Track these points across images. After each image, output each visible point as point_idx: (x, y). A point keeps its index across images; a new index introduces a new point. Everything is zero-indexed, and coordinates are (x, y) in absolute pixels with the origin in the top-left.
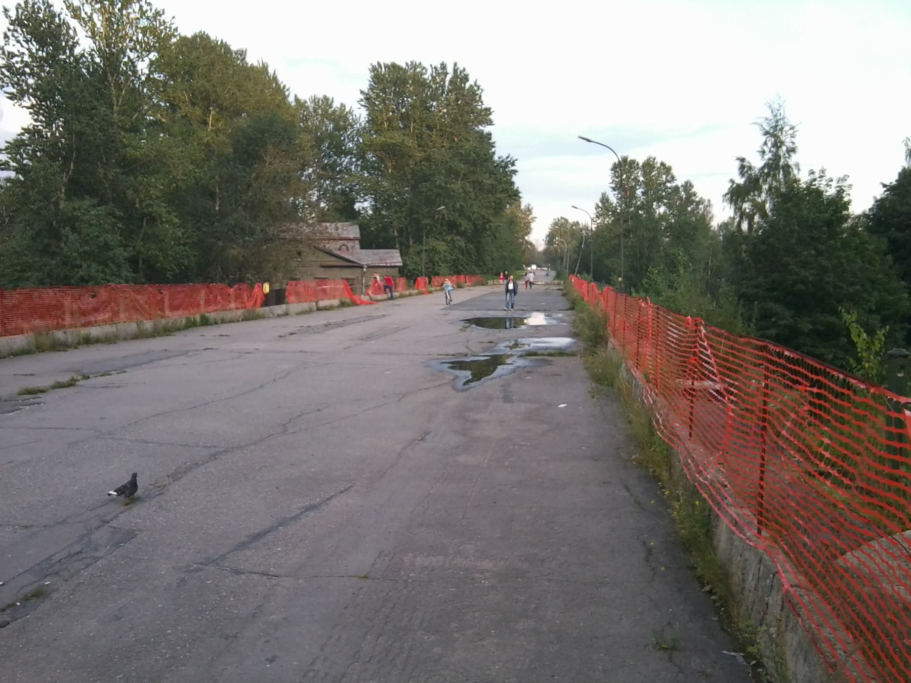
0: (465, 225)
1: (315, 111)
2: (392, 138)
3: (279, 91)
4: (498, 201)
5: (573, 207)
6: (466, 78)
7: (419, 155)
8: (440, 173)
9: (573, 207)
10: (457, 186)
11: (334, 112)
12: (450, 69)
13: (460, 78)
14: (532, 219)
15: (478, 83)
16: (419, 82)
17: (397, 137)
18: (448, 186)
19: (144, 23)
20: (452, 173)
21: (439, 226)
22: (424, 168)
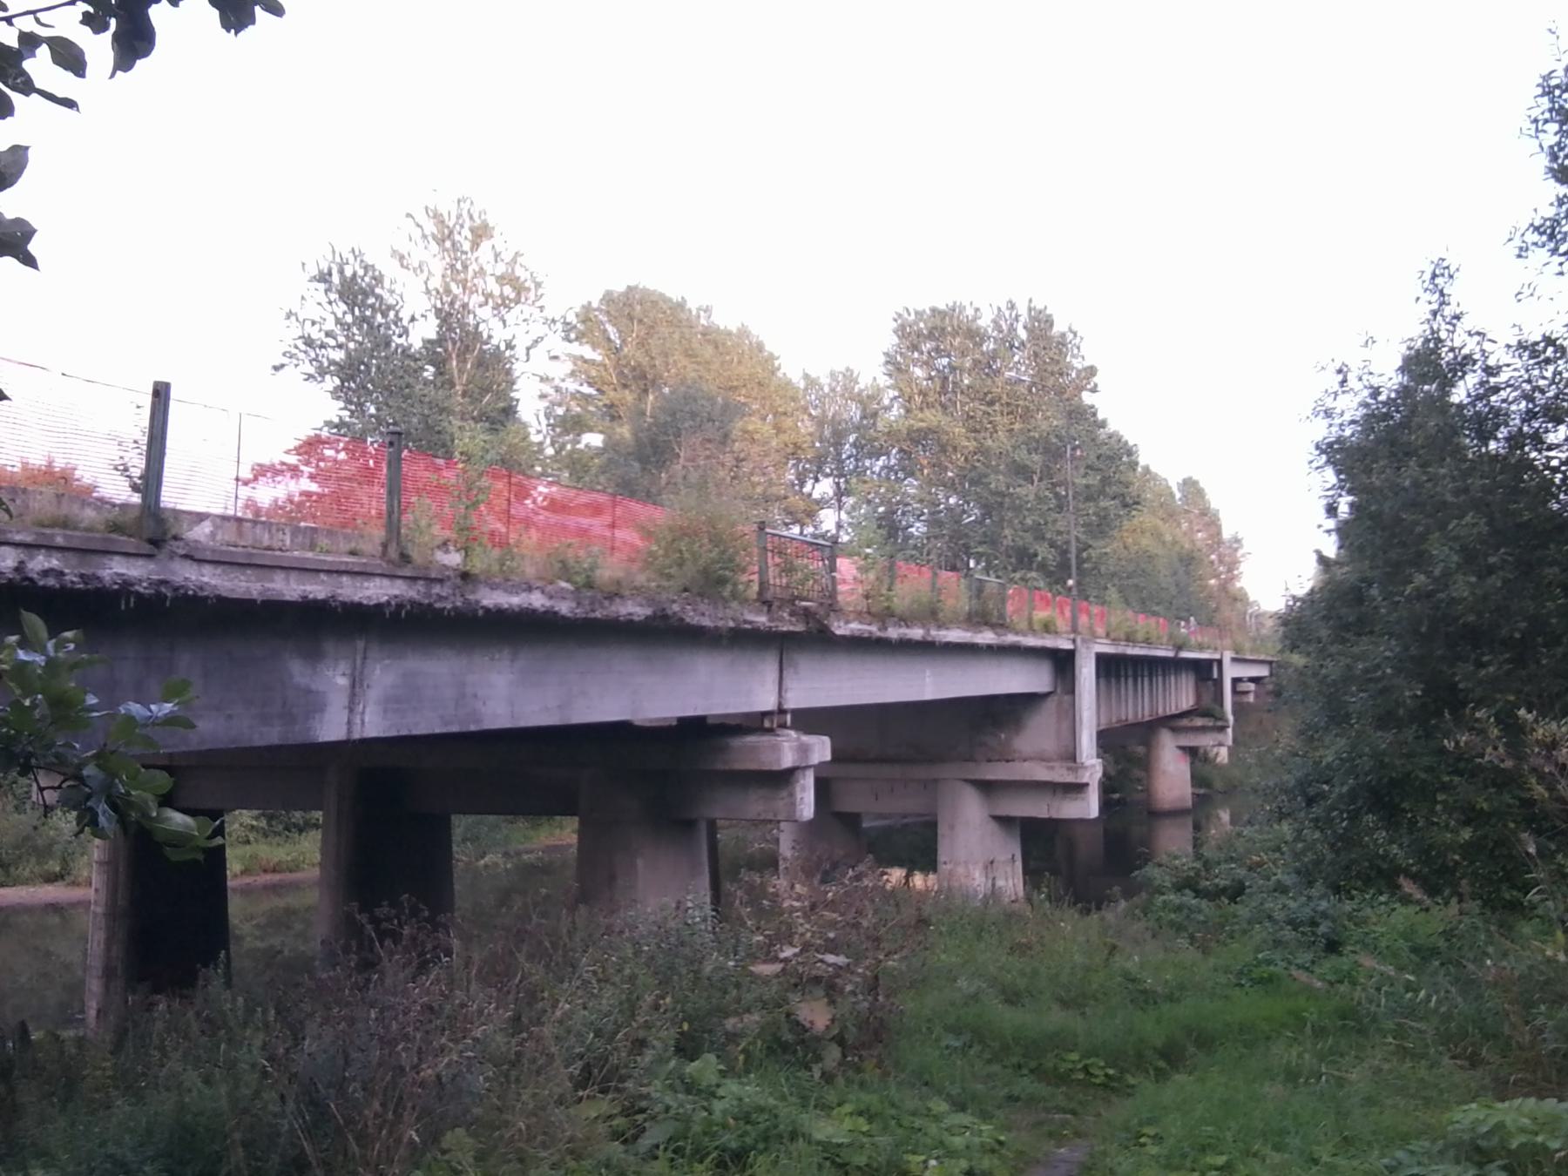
0: (1043, 551)
1: (833, 390)
2: (922, 420)
3: (769, 363)
4: (1102, 514)
5: (161, 394)
6: (1049, 322)
7: (972, 445)
8: (997, 472)
9: (161, 394)
10: (1027, 491)
11: (861, 391)
12: (1022, 310)
13: (1041, 323)
14: (1243, 556)
15: (1074, 328)
16: (974, 335)
17: (932, 417)
18: (1011, 490)
19: (501, 269)
20: (1022, 472)
21: (1004, 558)
22: (977, 464)
